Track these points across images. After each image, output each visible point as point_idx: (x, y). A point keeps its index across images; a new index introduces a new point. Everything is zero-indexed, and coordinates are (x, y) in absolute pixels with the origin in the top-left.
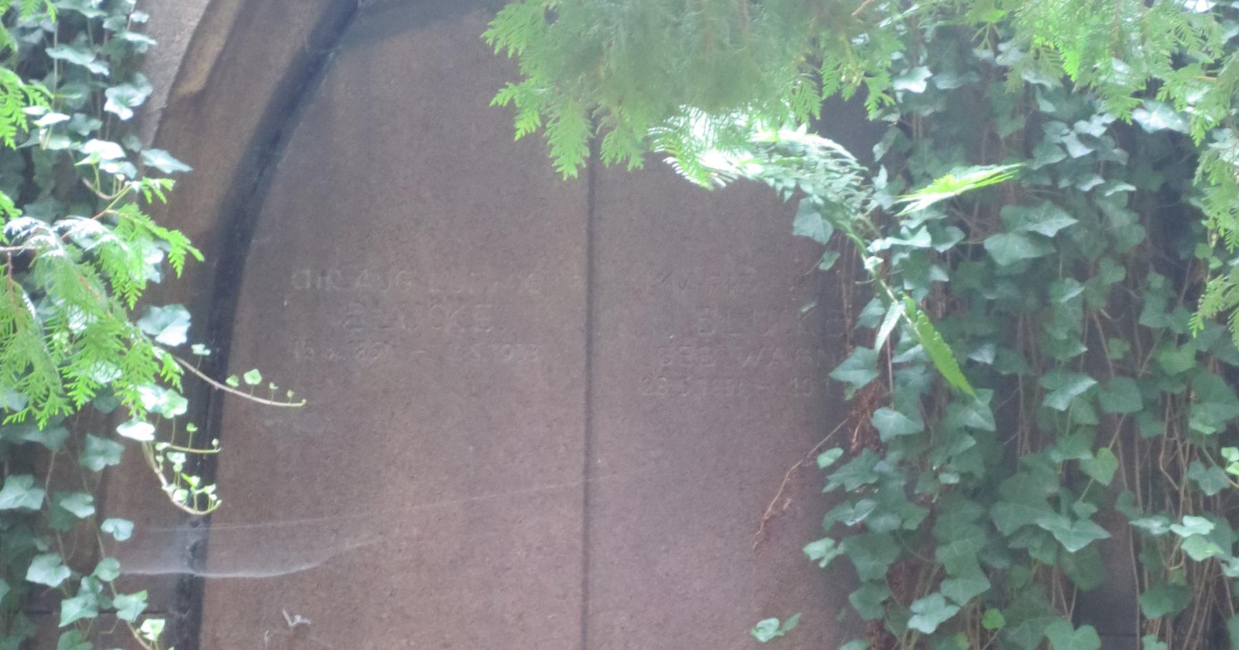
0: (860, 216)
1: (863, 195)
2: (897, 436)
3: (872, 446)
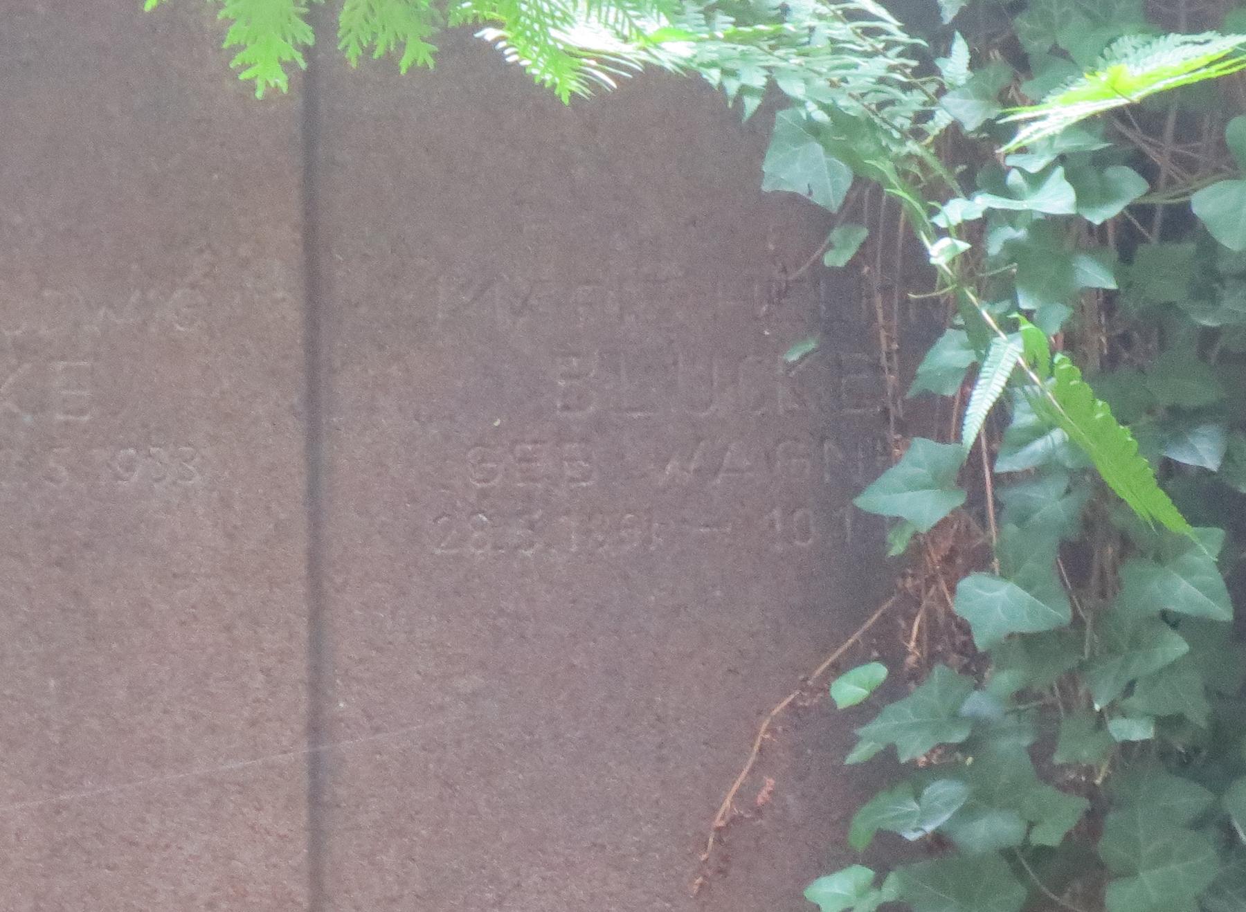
0: (912, 147)
1: (915, 100)
2: (1011, 636)
3: (954, 657)
